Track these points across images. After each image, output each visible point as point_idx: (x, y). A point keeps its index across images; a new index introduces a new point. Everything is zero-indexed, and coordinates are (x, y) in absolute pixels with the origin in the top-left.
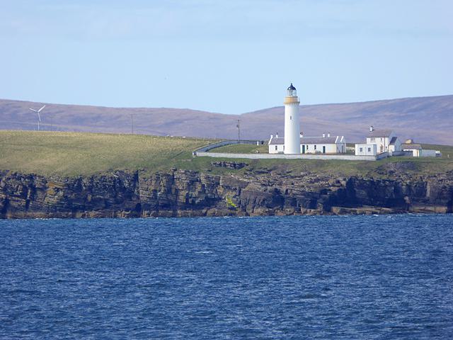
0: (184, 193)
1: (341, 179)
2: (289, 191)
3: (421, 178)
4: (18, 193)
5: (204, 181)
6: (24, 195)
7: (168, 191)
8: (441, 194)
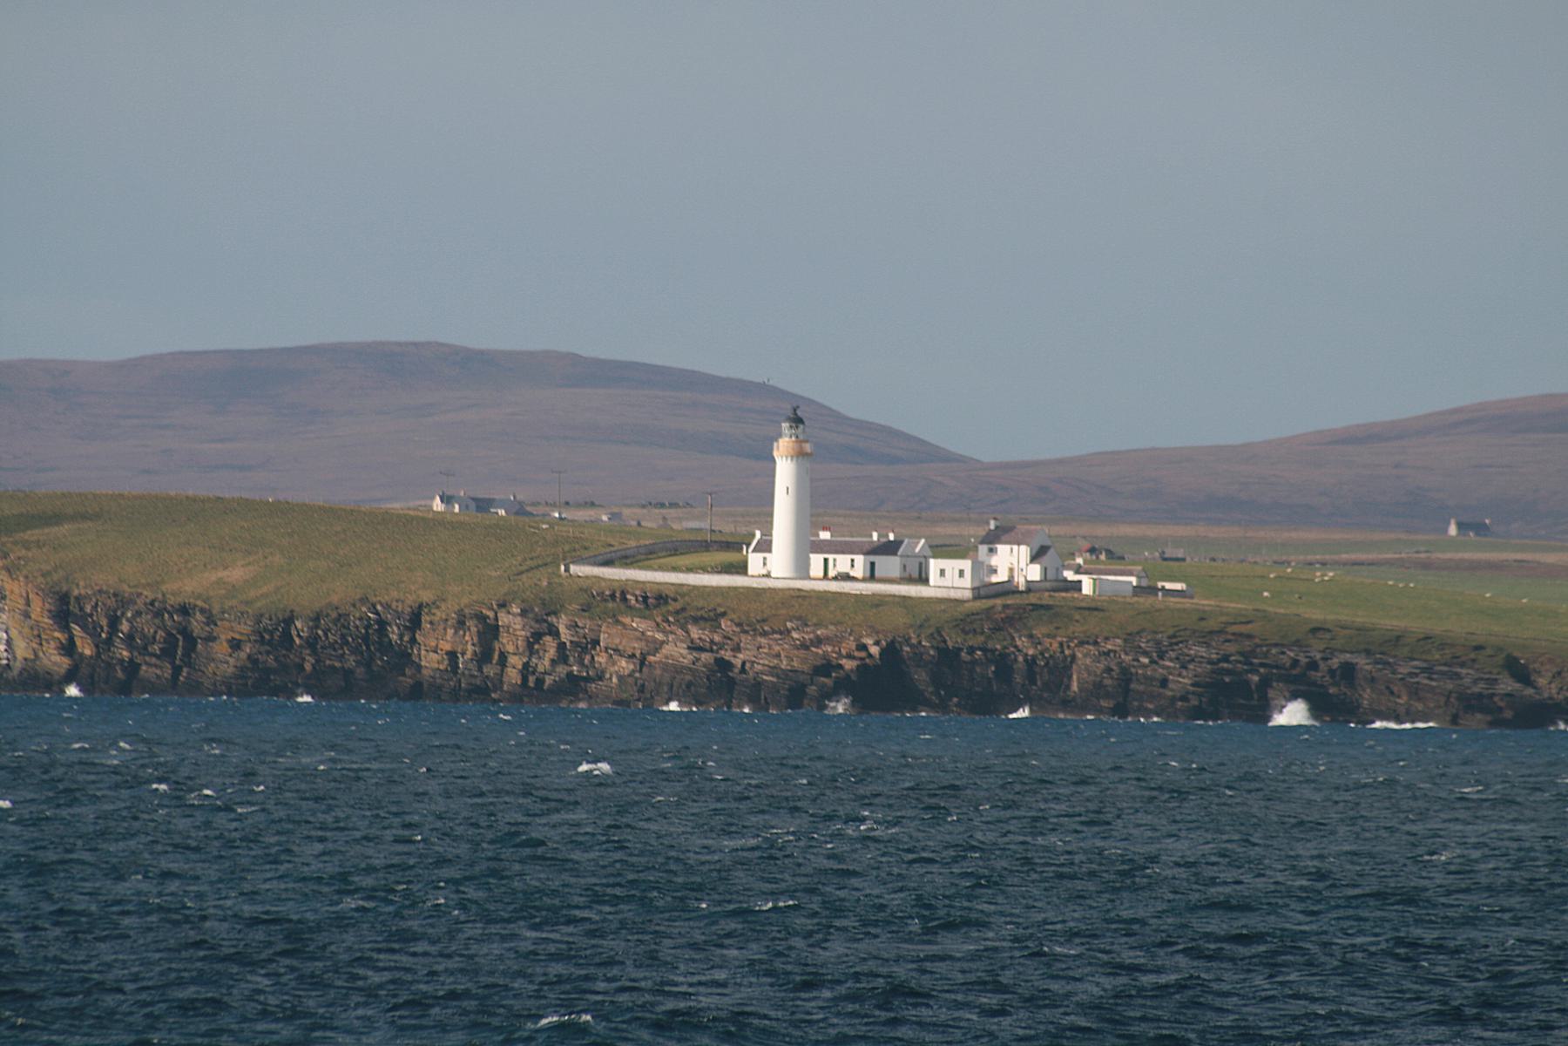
0: (516, 661)
1: (869, 641)
2: (748, 665)
3: (1061, 645)
4: (156, 648)
5: (565, 635)
6: (168, 652)
7: (484, 657)
8: (1099, 686)
